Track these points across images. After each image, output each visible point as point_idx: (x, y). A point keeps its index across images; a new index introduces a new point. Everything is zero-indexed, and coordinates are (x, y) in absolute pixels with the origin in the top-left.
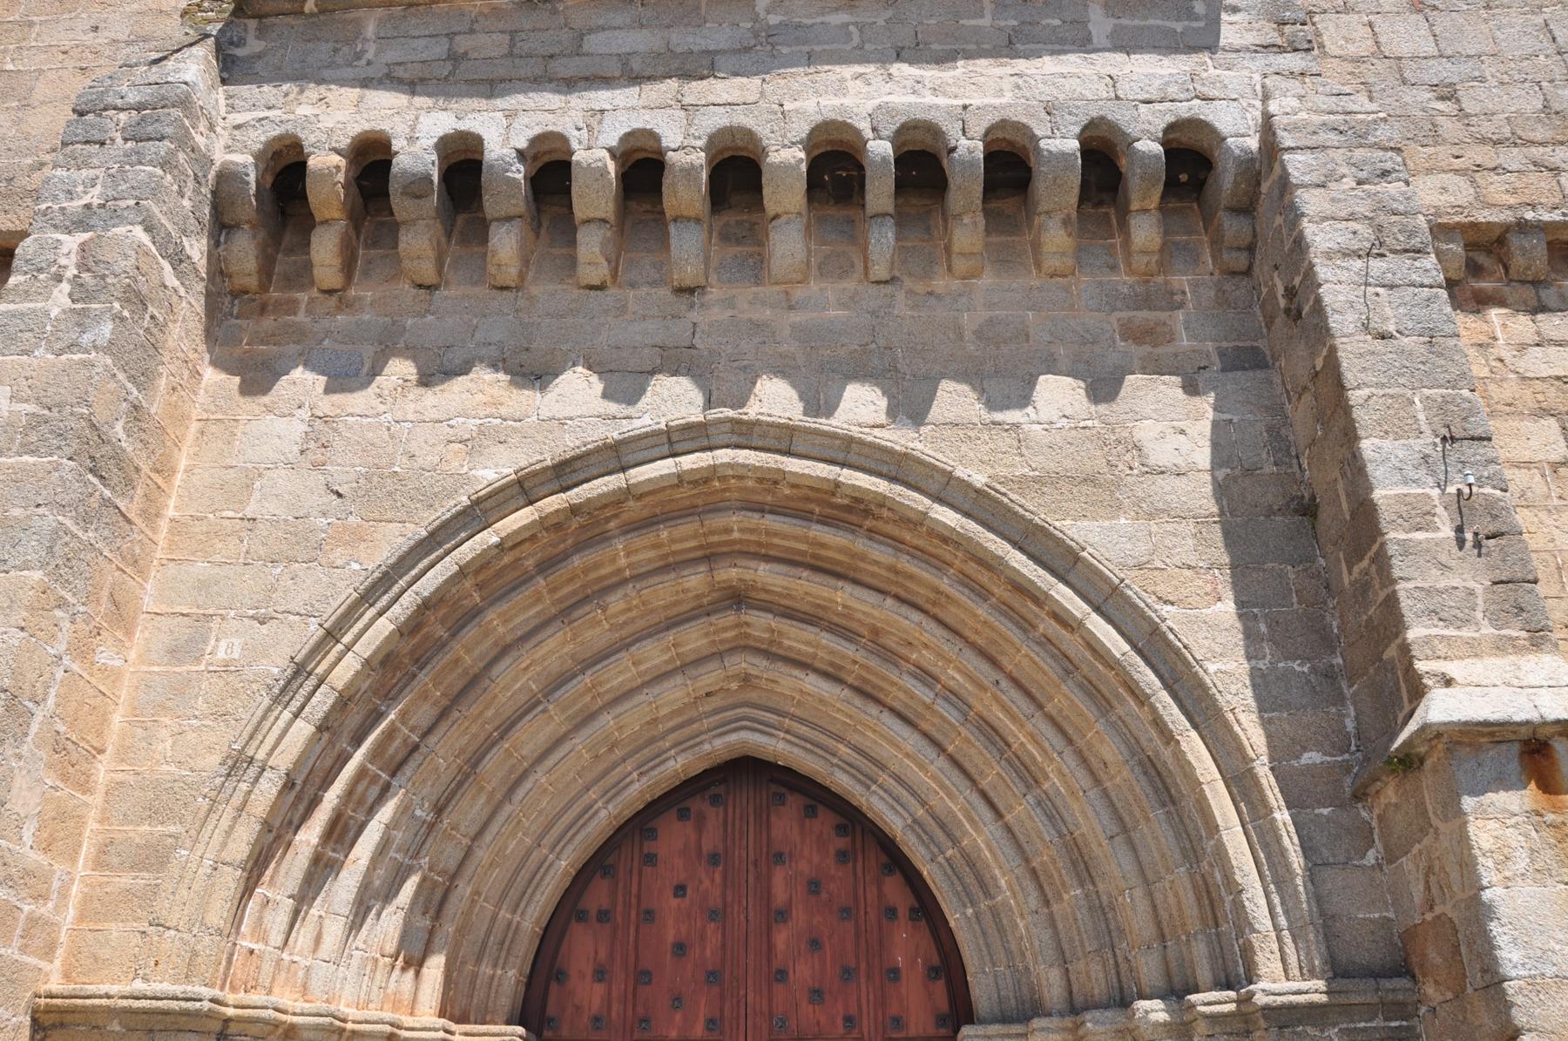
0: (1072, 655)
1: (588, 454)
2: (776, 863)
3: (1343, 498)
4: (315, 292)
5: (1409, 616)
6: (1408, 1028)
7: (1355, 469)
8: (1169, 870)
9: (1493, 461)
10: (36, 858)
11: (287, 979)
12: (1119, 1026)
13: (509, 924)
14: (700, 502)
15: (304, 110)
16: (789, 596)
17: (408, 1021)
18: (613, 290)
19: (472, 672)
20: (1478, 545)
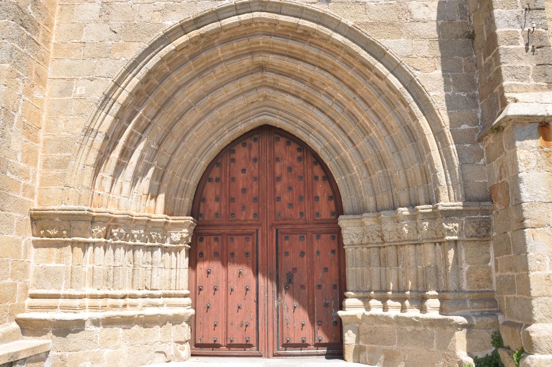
1: (206, 14)
2: (276, 161)
3: (485, 32)
5: (504, 76)
6: (488, 218)
7: (491, 21)
8: (412, 165)
9: (544, 18)
10: (23, 165)
11: (112, 203)
12: (393, 216)
13: (186, 183)
14: (248, 32)
17: (153, 216)
19: (168, 96)
20: (533, 51)
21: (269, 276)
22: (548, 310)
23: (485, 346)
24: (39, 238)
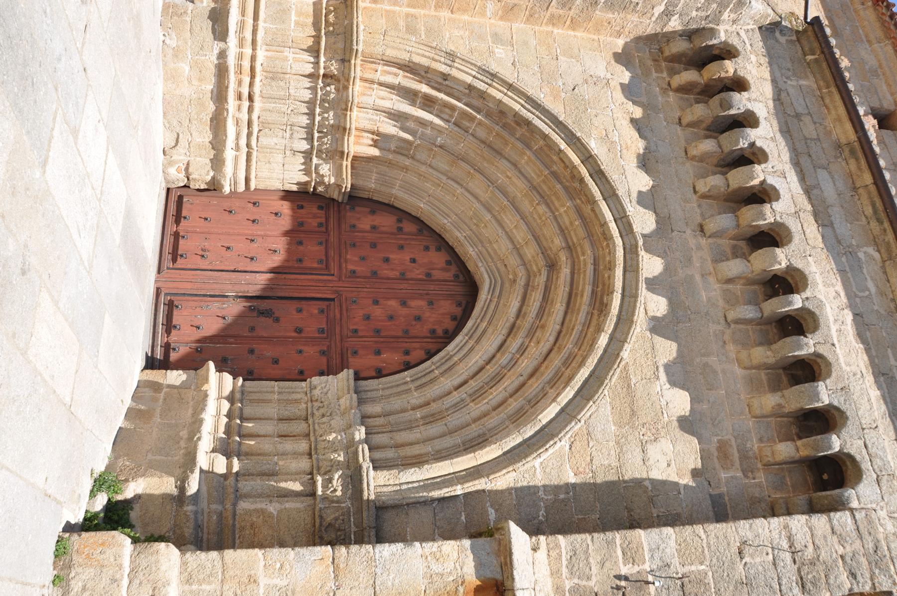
0: (539, 404)
1: (609, 183)
4: (668, 79)
15: (753, 58)
16: (556, 288)
17: (352, 139)
18: (695, 197)
20: (618, 588)
21: (269, 287)
22: (201, 577)
23: (147, 525)
24: (324, 6)
